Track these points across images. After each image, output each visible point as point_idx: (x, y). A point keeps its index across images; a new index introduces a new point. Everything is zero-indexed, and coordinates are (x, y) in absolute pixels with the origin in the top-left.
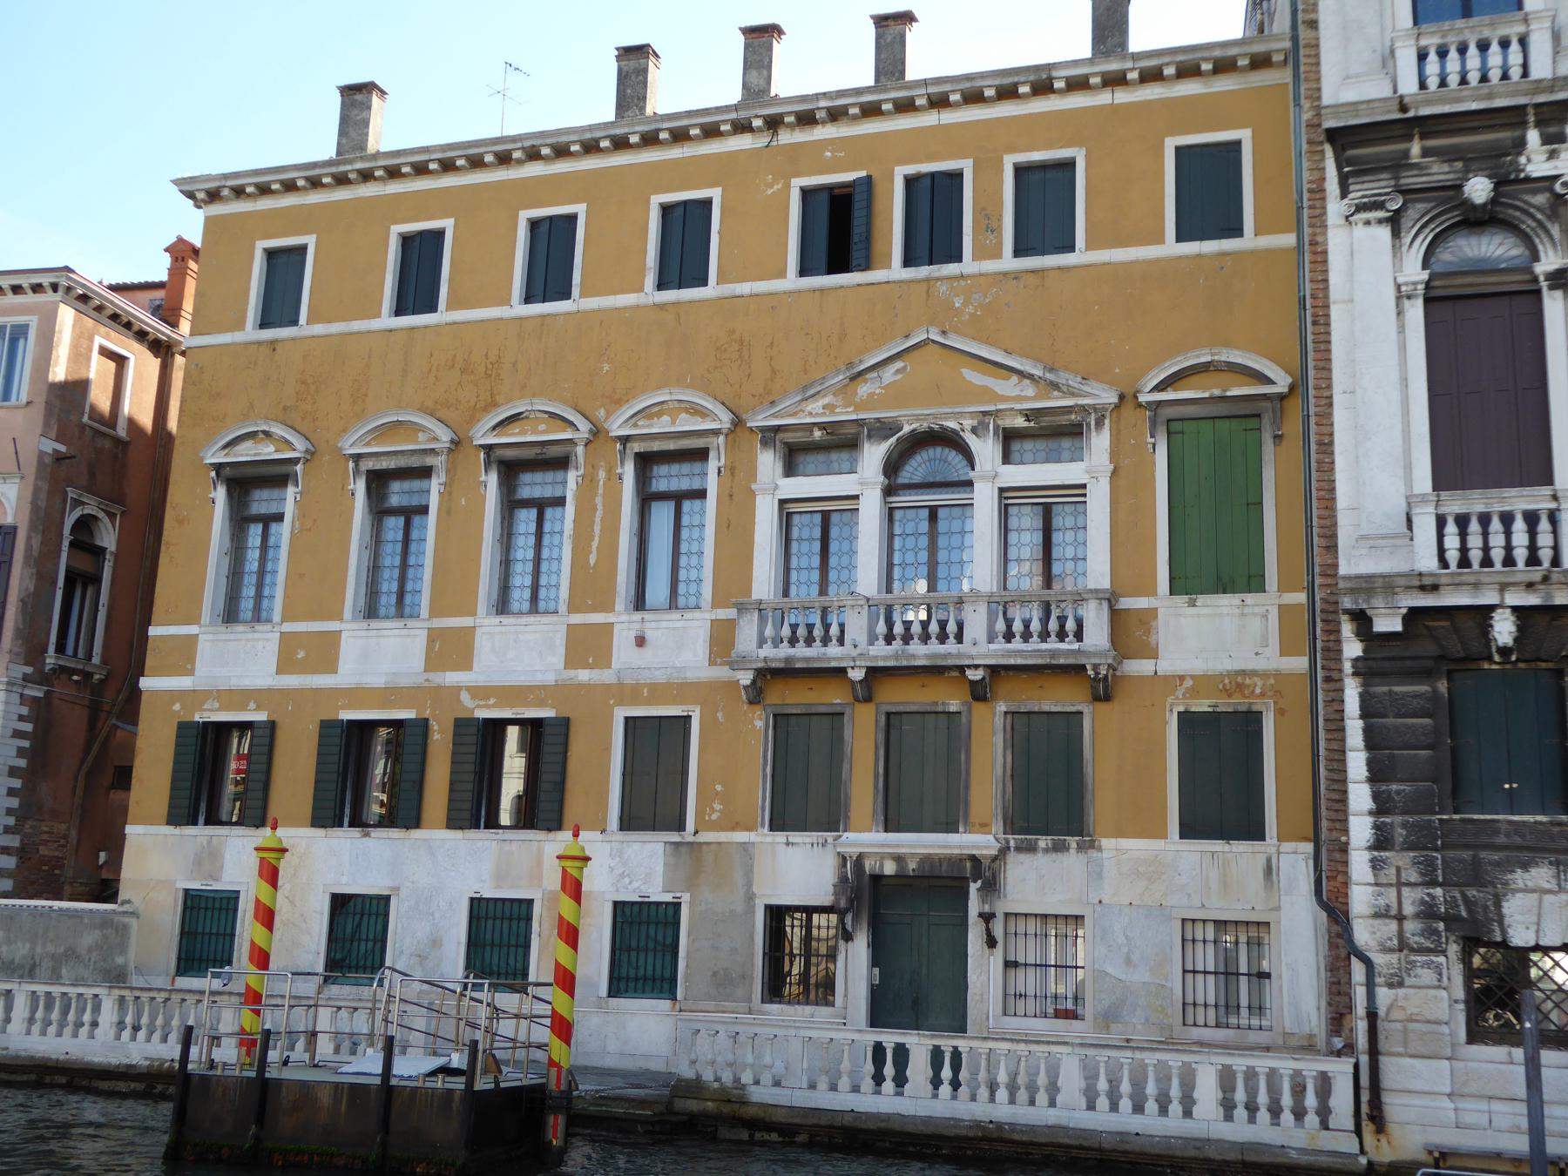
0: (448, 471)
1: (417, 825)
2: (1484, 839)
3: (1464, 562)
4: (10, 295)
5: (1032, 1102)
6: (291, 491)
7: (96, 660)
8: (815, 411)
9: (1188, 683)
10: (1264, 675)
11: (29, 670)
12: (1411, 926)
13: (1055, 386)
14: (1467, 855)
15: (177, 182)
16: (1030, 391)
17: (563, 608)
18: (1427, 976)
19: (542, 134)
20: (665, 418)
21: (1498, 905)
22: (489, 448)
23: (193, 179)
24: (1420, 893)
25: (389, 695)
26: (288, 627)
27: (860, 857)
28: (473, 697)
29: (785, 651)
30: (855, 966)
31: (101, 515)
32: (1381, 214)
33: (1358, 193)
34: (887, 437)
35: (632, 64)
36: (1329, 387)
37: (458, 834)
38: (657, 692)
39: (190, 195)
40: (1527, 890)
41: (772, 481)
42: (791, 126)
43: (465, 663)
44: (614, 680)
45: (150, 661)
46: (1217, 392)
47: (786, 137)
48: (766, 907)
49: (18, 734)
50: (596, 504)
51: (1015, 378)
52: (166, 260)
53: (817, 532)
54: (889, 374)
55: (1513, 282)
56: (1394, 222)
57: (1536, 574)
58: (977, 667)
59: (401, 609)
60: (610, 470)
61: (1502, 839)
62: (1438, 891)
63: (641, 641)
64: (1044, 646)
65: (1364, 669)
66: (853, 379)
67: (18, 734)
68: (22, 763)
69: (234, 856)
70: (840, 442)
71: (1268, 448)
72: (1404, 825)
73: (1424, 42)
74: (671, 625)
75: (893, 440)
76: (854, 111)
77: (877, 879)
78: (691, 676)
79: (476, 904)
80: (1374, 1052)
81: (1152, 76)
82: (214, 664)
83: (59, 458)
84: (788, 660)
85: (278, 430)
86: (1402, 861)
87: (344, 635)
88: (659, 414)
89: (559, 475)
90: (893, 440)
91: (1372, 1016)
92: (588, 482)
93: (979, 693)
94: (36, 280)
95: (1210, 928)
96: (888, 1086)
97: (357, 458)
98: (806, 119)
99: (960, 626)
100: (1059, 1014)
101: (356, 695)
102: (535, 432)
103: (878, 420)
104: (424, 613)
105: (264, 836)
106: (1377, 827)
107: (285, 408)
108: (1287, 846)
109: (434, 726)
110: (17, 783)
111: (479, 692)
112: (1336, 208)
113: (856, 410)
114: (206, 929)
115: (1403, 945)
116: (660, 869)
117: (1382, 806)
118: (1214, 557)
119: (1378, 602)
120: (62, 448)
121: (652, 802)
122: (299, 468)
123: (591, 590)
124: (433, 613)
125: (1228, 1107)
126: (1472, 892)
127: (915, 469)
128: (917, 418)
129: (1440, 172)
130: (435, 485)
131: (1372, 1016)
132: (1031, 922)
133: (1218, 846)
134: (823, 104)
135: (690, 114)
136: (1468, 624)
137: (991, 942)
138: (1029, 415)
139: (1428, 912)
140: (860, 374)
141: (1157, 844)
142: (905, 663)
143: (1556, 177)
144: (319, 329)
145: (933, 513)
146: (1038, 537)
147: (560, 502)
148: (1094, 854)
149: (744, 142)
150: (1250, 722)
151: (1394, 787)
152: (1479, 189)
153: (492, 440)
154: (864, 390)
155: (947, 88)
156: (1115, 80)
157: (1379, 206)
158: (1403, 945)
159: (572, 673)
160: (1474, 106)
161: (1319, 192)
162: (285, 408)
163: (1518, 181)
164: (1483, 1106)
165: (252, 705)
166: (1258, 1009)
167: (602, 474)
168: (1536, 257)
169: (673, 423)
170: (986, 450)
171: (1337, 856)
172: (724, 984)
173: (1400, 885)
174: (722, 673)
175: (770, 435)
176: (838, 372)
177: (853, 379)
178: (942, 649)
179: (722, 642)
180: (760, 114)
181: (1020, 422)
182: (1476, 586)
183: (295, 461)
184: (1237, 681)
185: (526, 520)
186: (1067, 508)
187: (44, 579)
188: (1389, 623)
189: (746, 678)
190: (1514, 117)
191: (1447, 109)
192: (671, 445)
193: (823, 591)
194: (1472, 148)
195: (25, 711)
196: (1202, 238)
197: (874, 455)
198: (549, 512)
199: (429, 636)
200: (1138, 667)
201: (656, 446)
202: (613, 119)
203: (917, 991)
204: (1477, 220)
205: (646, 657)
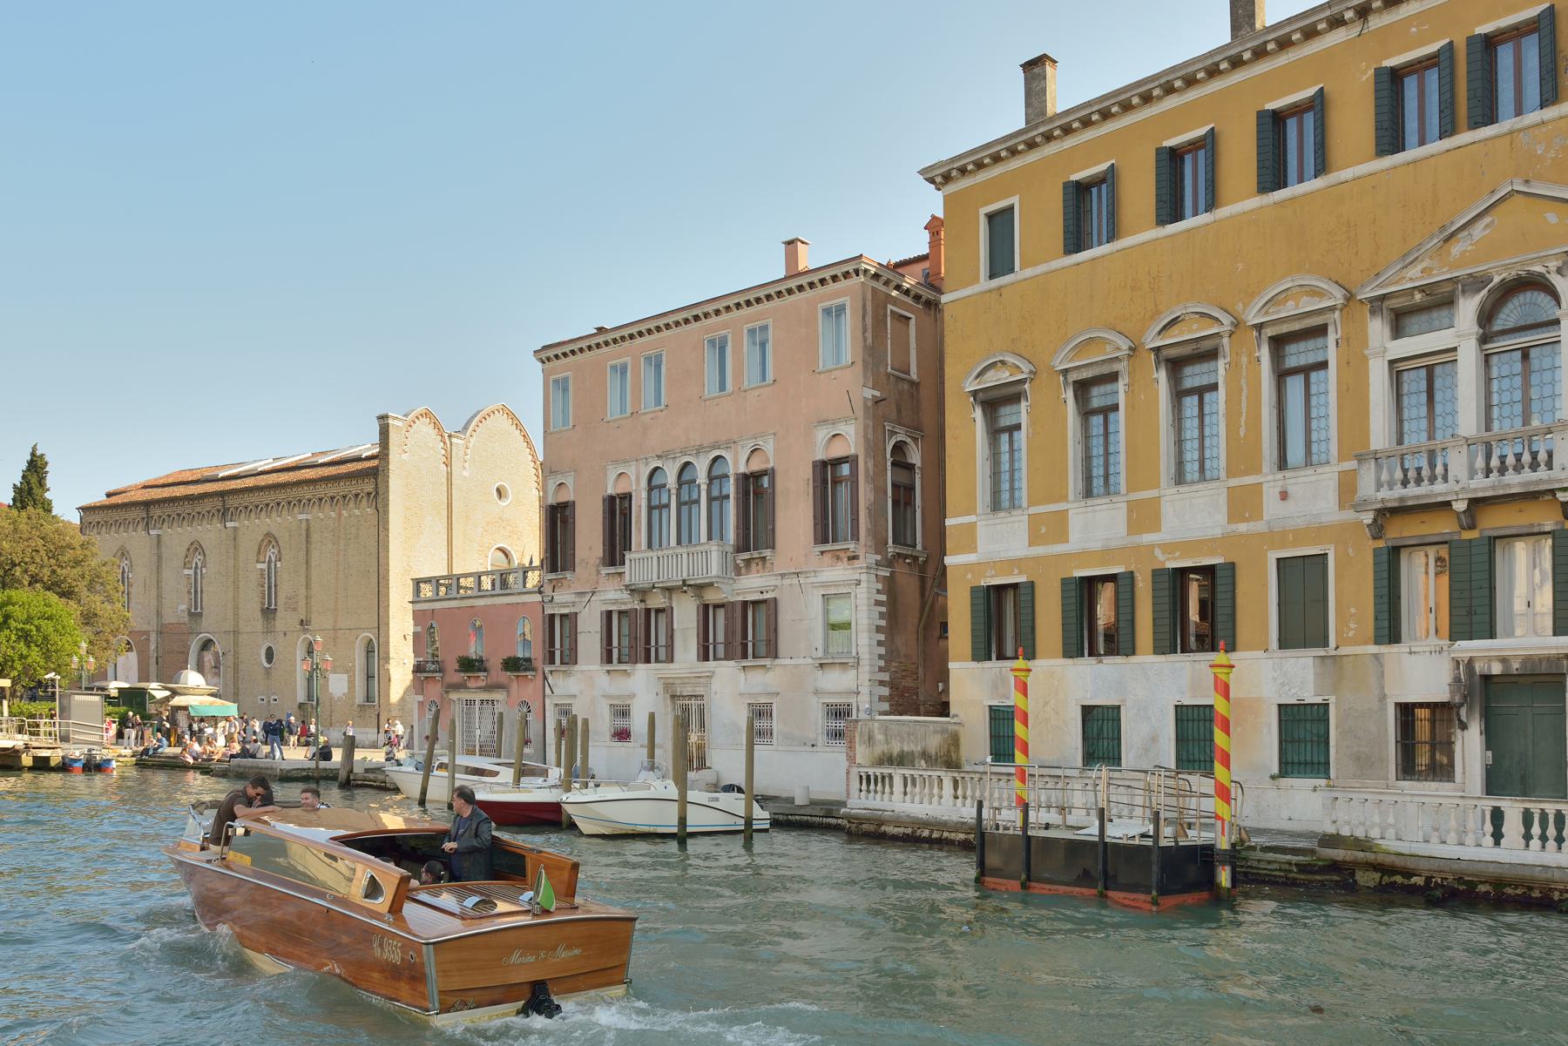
1: (1134, 653)
7: (919, 547)
8: (1415, 276)
11: (879, 557)
17: (1223, 475)
19: (1173, 69)
20: (1291, 303)
22: (1157, 350)
25: (1107, 554)
26: (1032, 510)
27: (1471, 660)
29: (1399, 491)
30: (1470, 747)
31: (909, 440)
34: (1479, 290)
38: (1299, 536)
39: (932, 181)
43: (1155, 526)
48: (1397, 704)
49: (878, 603)
52: (926, 235)
53: (1423, 385)
54: (1478, 230)
59: (1108, 489)
63: (1284, 496)
66: (1446, 240)
67: (878, 603)
68: (883, 623)
70: (1439, 300)
74: (1306, 479)
77: (1487, 678)
78: (1325, 520)
79: (1180, 709)
81: (1284, 44)
82: (988, 544)
83: (877, 401)
84: (1402, 499)
85: (1010, 359)
88: (1286, 300)
89: (1212, 364)
94: (845, 268)
99: (1550, 454)
101: (1083, 556)
102: (1190, 331)
105: (1220, 657)
109: (1138, 577)
110: (882, 637)
116: (1311, 678)
120: (878, 394)
121: (1302, 626)
122: (1027, 386)
123: (1241, 459)
124: (1131, 488)
127: (1509, 316)
128: (1506, 267)
130: (1121, 386)
135: (1290, 21)
140: (1452, 235)
142: (1501, 492)
145: (1525, 354)
147: (1324, 365)
149: (1340, 36)
154: (1456, 249)
155: (1287, 30)
156: (1260, 53)
159: (1233, 527)
172: (1365, 764)
174: (1350, 515)
176: (1432, 237)
177: (1446, 240)
178: (1534, 476)
183: (1022, 381)
185: (1295, 385)
187: (879, 491)
189: (1368, 518)
192: (1297, 326)
195: (880, 586)
197: (1468, 308)
205: (1290, 508)
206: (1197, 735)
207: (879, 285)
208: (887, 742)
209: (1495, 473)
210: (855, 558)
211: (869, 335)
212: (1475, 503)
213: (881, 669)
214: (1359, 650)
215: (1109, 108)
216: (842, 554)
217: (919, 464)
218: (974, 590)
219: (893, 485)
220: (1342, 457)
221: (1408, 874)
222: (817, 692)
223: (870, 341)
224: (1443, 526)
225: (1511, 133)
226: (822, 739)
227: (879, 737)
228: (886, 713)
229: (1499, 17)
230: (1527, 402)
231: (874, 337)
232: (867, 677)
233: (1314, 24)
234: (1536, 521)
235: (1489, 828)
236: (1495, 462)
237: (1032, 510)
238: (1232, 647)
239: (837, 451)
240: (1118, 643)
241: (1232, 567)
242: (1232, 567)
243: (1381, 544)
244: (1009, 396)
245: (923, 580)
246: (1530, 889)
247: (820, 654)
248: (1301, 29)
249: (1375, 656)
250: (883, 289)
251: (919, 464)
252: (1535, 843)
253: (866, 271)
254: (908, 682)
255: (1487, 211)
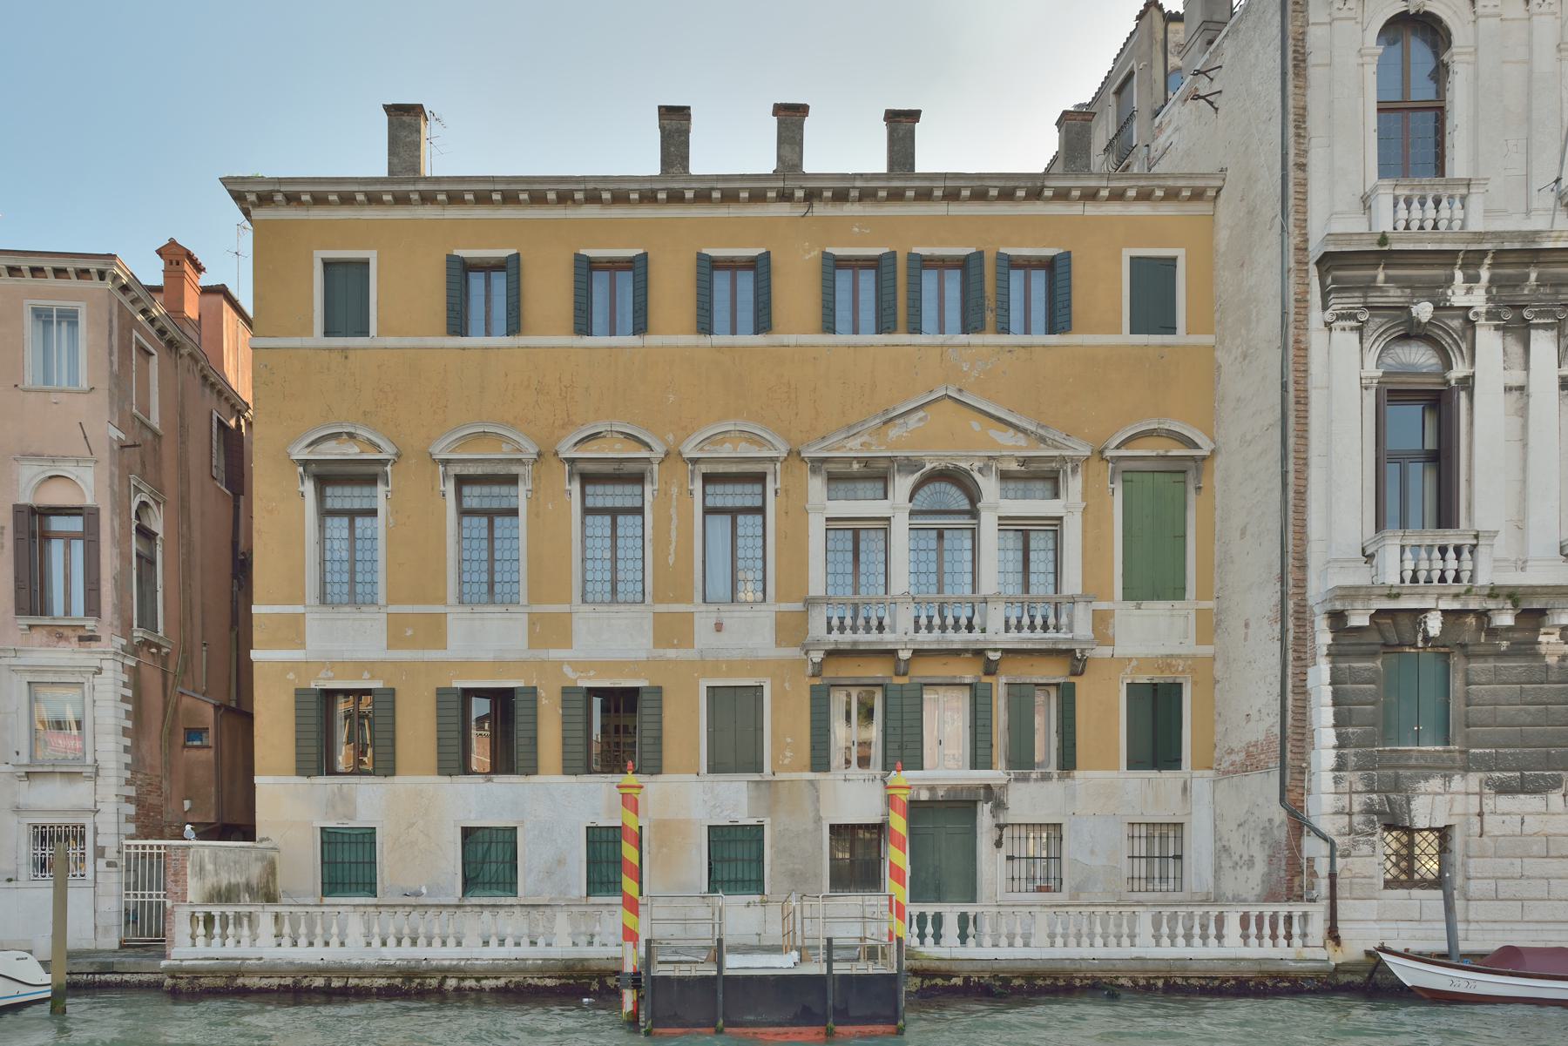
0: (534, 479)
2: (1402, 762)
3: (1415, 579)
4: (51, 277)
5: (1119, 945)
6: (381, 489)
7: (161, 634)
8: (854, 448)
9: (1134, 663)
10: (1186, 658)
11: (124, 642)
12: (1357, 819)
13: (1043, 439)
14: (1390, 772)
15: (225, 181)
16: (1021, 440)
17: (523, 599)
18: (1366, 849)
19: (605, 179)
20: (728, 446)
21: (1409, 803)
22: (572, 461)
23: (244, 180)
24: (1364, 798)
25: (499, 666)
26: (393, 609)
28: (575, 670)
29: (849, 636)
31: (152, 503)
32: (1354, 324)
33: (1338, 304)
34: (913, 472)
35: (673, 124)
36: (1306, 451)
37: (573, 778)
38: (733, 667)
39: (238, 197)
40: (1426, 793)
41: (822, 504)
42: (827, 201)
43: (566, 642)
44: (697, 657)
45: (257, 636)
46: (1162, 452)
47: (820, 210)
50: (550, 511)
51: (1011, 431)
52: (160, 264)
53: (849, 546)
54: (913, 420)
55: (1432, 384)
56: (1360, 330)
57: (1456, 588)
58: (996, 650)
60: (681, 486)
61: (1413, 762)
62: (1375, 796)
63: (719, 627)
64: (1047, 635)
65: (1334, 654)
67: (124, 699)
68: (129, 724)
69: (367, 801)
70: (877, 475)
71: (1192, 496)
72: (1355, 755)
73: (1398, 192)
75: (918, 475)
76: (882, 194)
80: (1333, 898)
81: (703, 197)
82: (306, 641)
84: (855, 643)
85: (363, 432)
86: (1354, 778)
87: (449, 617)
88: (723, 442)
90: (918, 475)
91: (1332, 876)
92: (663, 496)
93: (991, 669)
94: (36, 262)
95: (1144, 828)
96: (1212, 941)
97: (446, 462)
98: (841, 196)
100: (1040, 889)
101: (466, 666)
103: (907, 458)
104: (523, 599)
106: (1338, 756)
107: (365, 413)
108: (1198, 773)
110: (128, 742)
111: (577, 665)
112: (1316, 317)
113: (888, 449)
114: (348, 862)
115: (1352, 831)
117: (1342, 742)
118: (1155, 571)
119: (1358, 605)
120: (123, 436)
121: (735, 749)
122: (389, 468)
124: (534, 598)
125: (1157, 938)
126: (1393, 796)
128: (938, 458)
129: (1395, 296)
130: (522, 489)
131: (1332, 876)
132: (1016, 829)
133: (1153, 774)
134: (859, 184)
135: (743, 177)
136: (1405, 621)
137: (999, 844)
138: (1025, 461)
139: (1369, 810)
140: (891, 420)
141: (1113, 774)
143: (1470, 308)
144: (391, 341)
145: (940, 534)
146: (1020, 555)
148: (1068, 781)
149: (784, 210)
150: (1175, 689)
151: (1350, 730)
152: (1424, 311)
153: (305, 455)
154: (894, 432)
156: (676, 197)
157: (1353, 317)
158: (1352, 831)
159: (661, 652)
160: (1429, 247)
161: (1302, 301)
162: (365, 413)
163: (1445, 308)
164: (1393, 925)
165: (366, 675)
166: (1179, 878)
167: (675, 490)
168: (1448, 366)
169: (735, 450)
170: (989, 486)
171: (1298, 776)
172: (799, 881)
173: (1351, 792)
174: (795, 652)
175: (817, 464)
177: (885, 423)
178: (869, 637)
179: (790, 629)
180: (789, 184)
181: (1014, 466)
182: (1423, 595)
183: (384, 462)
184: (1167, 661)
186: (1042, 535)
187: (124, 557)
188: (1359, 619)
189: (817, 656)
190: (1446, 258)
191: (1411, 247)
192: (734, 469)
193: (940, 590)
194: (1420, 279)
195: (126, 678)
196: (1149, 332)
197: (902, 485)
198: (621, 519)
199: (530, 620)
200: (1103, 652)
201: (721, 468)
202: (658, 172)
203: (944, 871)
204: (1413, 333)
206: (607, 860)
207: (125, 300)
208: (217, 874)
209: (848, 631)
210: (93, 638)
211: (115, 358)
212: (916, 652)
213: (128, 782)
214: (795, 776)
215: (517, 192)
216: (67, 632)
217: (161, 535)
218: (301, 694)
219: (138, 555)
220: (779, 598)
221: (948, 976)
222: (17, 810)
223: (116, 367)
224: (878, 671)
225: (942, 346)
226: (26, 871)
227: (209, 867)
228: (132, 837)
229: (933, 245)
230: (940, 573)
231: (121, 364)
232: (114, 791)
233: (765, 189)
234: (957, 674)
235: (915, 930)
236: (861, 622)
237: (393, 609)
238: (655, 767)
239: (56, 496)
240: (510, 757)
241: (658, 690)
242: (658, 690)
243: (817, 681)
244: (365, 475)
245: (165, 674)
246: (1056, 979)
247: (24, 759)
248: (751, 190)
249: (811, 782)
250: (129, 306)
251: (161, 535)
252: (1253, 941)
253: (116, 277)
254: (153, 799)
255: (922, 407)
